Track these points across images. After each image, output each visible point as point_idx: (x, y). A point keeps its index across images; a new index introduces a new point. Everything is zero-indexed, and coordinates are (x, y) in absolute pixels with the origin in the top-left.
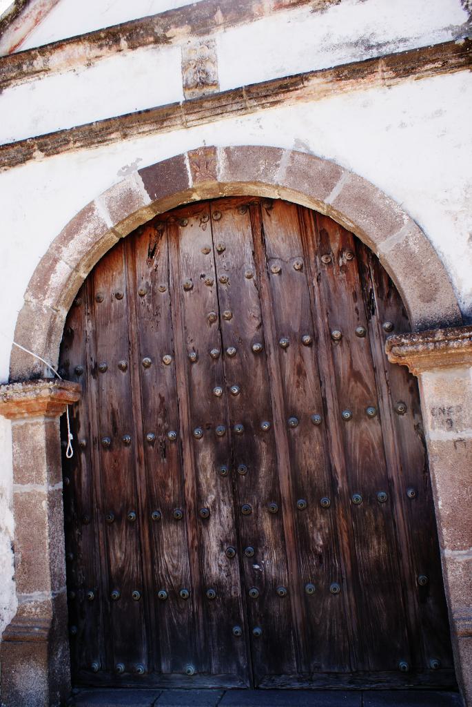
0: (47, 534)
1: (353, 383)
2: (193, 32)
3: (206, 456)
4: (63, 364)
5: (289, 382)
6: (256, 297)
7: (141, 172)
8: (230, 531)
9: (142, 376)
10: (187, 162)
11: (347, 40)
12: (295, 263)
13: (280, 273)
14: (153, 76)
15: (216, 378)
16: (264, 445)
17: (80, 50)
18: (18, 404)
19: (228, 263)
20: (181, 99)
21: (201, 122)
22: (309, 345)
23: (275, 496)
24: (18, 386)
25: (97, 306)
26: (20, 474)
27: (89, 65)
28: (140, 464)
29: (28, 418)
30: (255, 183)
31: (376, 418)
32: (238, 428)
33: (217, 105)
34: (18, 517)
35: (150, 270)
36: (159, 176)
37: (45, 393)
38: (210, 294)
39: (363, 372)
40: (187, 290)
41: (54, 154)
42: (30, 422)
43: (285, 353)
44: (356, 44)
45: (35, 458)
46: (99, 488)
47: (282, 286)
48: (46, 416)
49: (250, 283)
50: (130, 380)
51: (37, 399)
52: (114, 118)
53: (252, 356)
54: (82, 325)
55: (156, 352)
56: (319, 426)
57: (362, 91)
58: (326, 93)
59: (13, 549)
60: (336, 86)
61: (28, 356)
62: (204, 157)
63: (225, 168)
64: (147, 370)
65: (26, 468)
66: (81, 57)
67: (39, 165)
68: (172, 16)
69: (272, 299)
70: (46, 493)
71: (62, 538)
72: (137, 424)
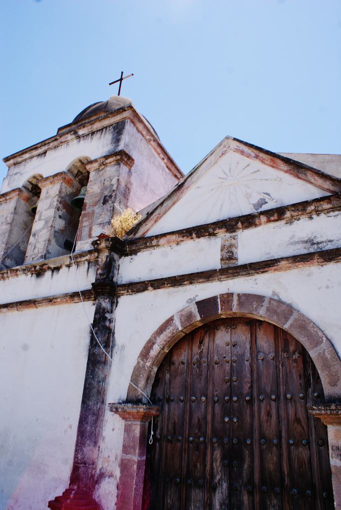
0: (134, 483)
1: (296, 425)
2: (227, 231)
3: (218, 454)
4: (153, 394)
5: (263, 419)
6: (250, 372)
7: (197, 303)
8: (226, 498)
9: (190, 406)
10: (219, 300)
11: (302, 239)
12: (270, 355)
13: (263, 360)
14: (206, 254)
15: (227, 412)
16: (247, 452)
17: (173, 237)
18: (129, 413)
19: (237, 352)
20: (218, 266)
21: (227, 279)
22: (275, 400)
23: (251, 481)
24: (130, 405)
25: (172, 367)
26: (126, 449)
27: (177, 244)
28: (185, 453)
29: (133, 421)
30: (251, 314)
31: (307, 446)
32: (235, 441)
33: (235, 272)
34: (122, 472)
35: (200, 351)
36: (205, 306)
37: (142, 410)
38: (227, 367)
39: (301, 418)
40: (216, 364)
41: (157, 289)
42: (133, 423)
43: (262, 404)
44: (306, 242)
45: (134, 441)
46: (163, 462)
47: (263, 367)
48: (141, 421)
49: (247, 363)
50: (184, 407)
51: (137, 413)
52: (186, 275)
53: (245, 403)
54: (164, 376)
55: (198, 395)
56: (276, 446)
57: (308, 268)
58: (289, 268)
59: (117, 488)
60: (294, 265)
61: (136, 389)
62: (227, 298)
63: (237, 305)
64: (193, 404)
65: (129, 446)
66: (174, 241)
67: (150, 294)
68: (218, 224)
69: (258, 373)
70: (136, 461)
71: (142, 486)
72: (186, 431)
